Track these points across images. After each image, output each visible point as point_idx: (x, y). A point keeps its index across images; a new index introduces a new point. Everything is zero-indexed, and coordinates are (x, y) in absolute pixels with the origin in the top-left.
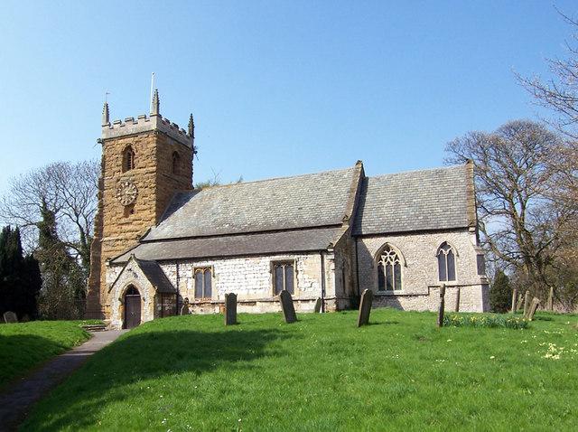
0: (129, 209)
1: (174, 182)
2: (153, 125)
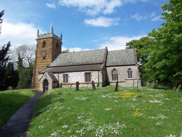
0: (44, 58)
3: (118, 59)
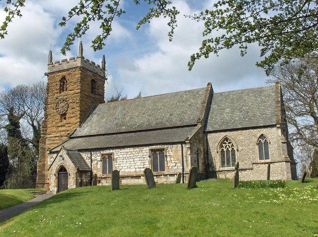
0: (63, 116)
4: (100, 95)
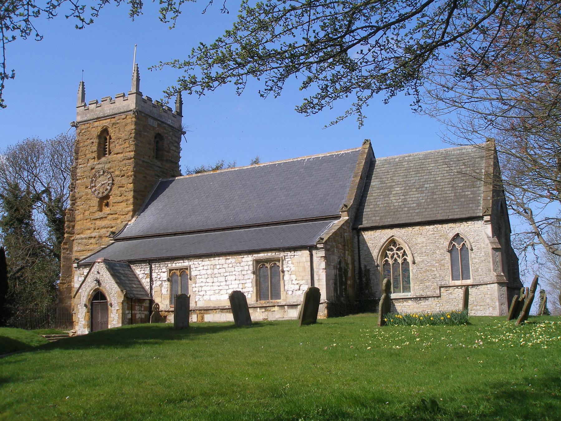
0: (104, 201)
1: (156, 168)
2: (131, 103)
3: (415, 195)
4: (172, 162)
